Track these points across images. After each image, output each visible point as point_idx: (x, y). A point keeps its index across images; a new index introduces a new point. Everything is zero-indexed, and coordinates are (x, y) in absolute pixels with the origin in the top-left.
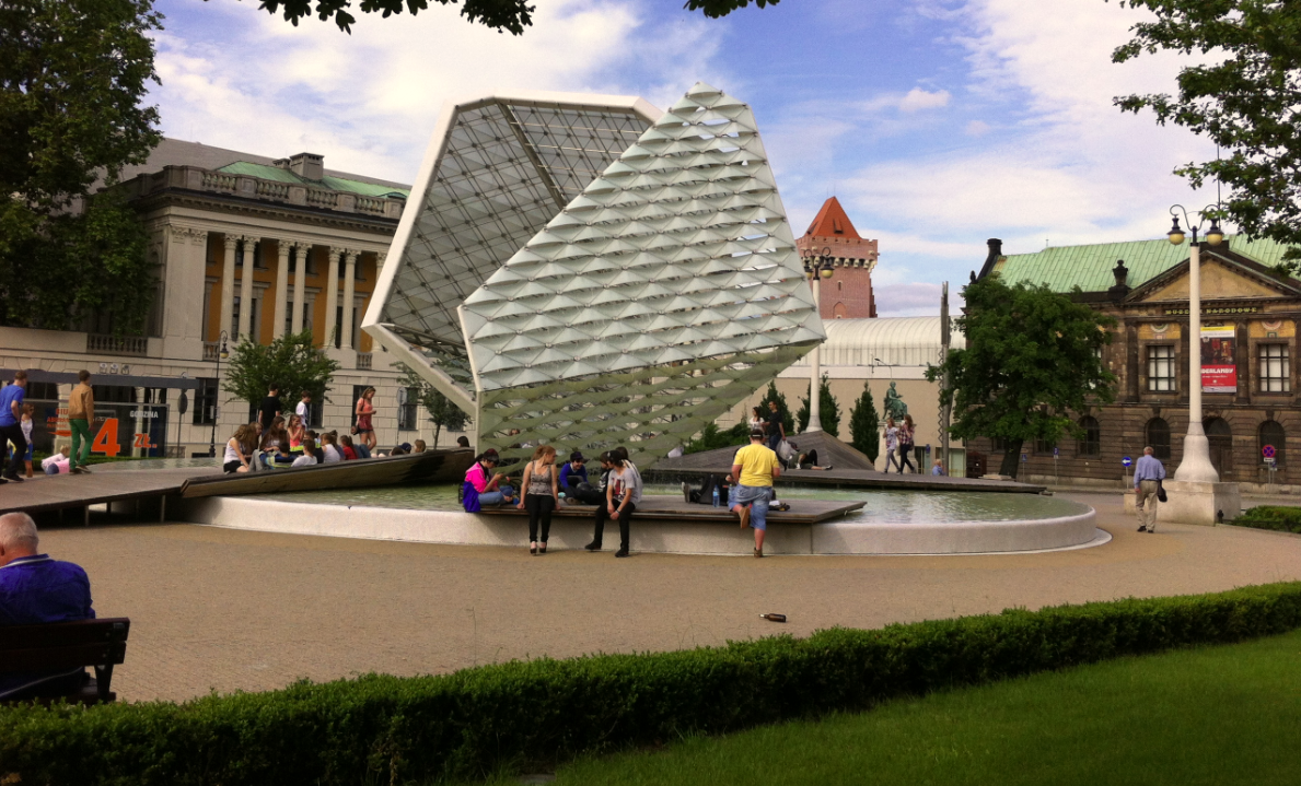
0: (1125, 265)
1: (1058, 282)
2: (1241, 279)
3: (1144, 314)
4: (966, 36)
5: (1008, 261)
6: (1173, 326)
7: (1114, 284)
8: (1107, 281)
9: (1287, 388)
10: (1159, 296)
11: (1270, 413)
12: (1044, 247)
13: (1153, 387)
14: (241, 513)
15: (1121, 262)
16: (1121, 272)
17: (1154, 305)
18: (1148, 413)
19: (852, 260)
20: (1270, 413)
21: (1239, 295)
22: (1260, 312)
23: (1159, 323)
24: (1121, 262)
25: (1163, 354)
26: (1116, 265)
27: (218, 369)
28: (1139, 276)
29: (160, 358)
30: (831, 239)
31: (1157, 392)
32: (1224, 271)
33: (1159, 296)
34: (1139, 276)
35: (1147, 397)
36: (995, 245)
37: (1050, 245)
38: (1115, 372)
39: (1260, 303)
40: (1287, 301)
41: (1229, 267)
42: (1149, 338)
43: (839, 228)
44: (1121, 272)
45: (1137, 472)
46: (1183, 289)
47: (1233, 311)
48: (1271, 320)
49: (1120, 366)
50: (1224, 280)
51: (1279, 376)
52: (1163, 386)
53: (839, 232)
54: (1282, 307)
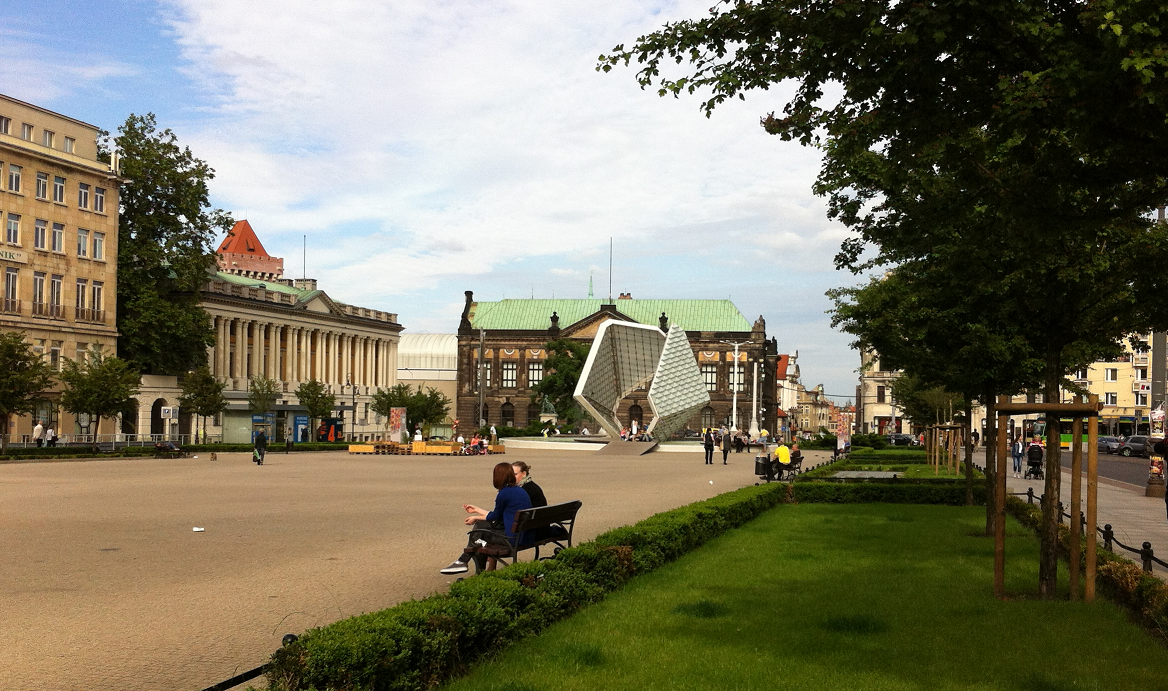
4: (177, 20)
5: (479, 305)
7: (550, 325)
8: (547, 324)
9: (714, 389)
10: (578, 335)
11: (636, 401)
12: (502, 299)
13: (505, 385)
14: (664, 448)
15: (555, 313)
16: (555, 319)
18: (528, 400)
19: (263, 274)
20: (636, 401)
24: (555, 313)
28: (563, 324)
30: (247, 256)
31: (507, 388)
33: (578, 335)
34: (563, 324)
36: (469, 294)
43: (252, 247)
44: (555, 319)
45: (497, 532)
46: (592, 331)
53: (252, 250)
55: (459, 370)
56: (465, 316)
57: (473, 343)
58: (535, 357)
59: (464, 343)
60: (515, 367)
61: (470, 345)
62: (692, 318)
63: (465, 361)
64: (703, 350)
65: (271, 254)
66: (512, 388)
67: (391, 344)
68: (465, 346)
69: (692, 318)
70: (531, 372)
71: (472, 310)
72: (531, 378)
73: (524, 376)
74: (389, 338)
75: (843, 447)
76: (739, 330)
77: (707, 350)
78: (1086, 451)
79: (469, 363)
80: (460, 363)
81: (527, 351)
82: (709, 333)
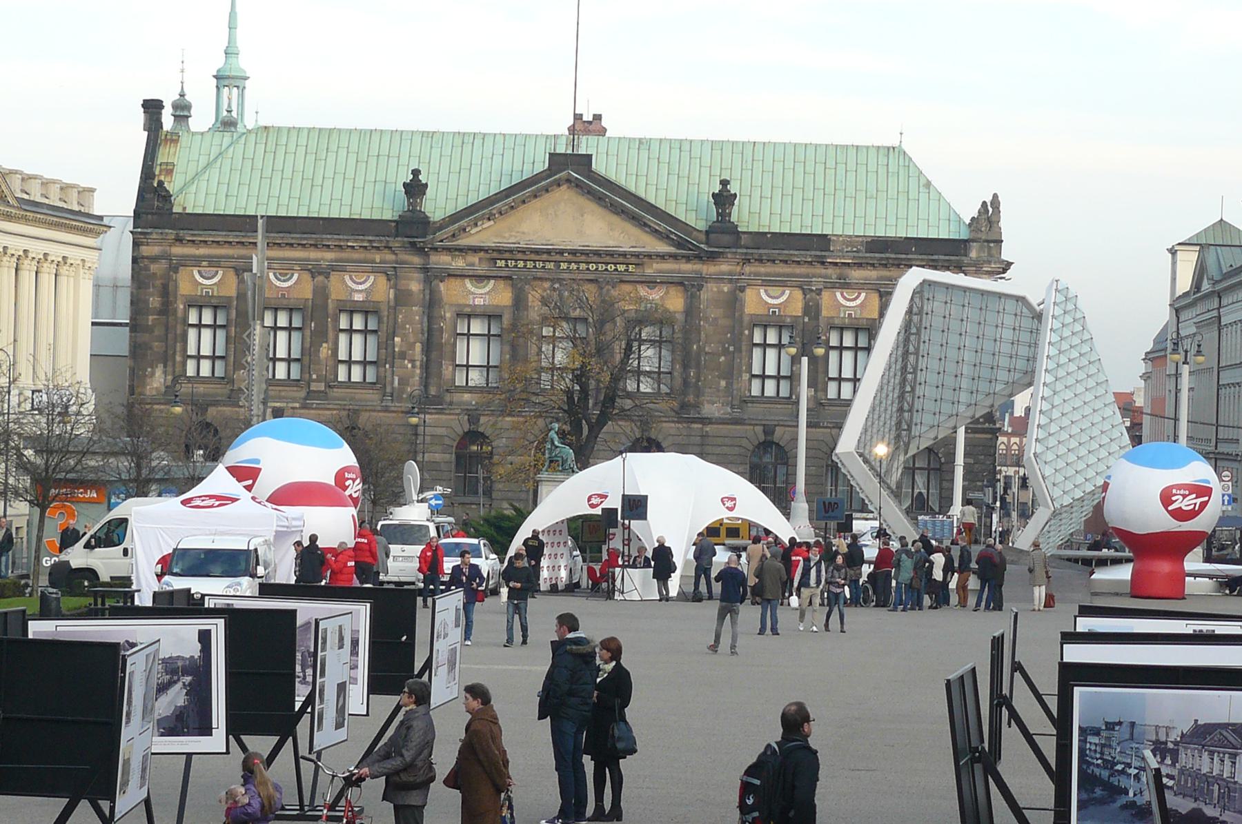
0: (733, 188)
1: (337, 195)
2: (615, 219)
3: (459, 263)
6: (501, 284)
10: (485, 234)
15: (416, 173)
16: (724, 199)
17: (475, 250)
18: (460, 425)
21: (611, 243)
22: (639, 271)
23: (479, 278)
24: (416, 173)
25: (477, 327)
26: (717, 188)
27: (468, 366)
28: (437, 206)
29: (522, 171)
31: (349, 384)
32: (591, 206)
34: (437, 206)
35: (457, 397)
37: (262, 123)
38: (403, 355)
39: (641, 258)
40: (688, 259)
41: (590, 193)
42: (462, 301)
44: (415, 188)
47: (601, 267)
48: (651, 283)
49: (412, 346)
50: (588, 217)
51: (202, 361)
52: (476, 378)
54: (669, 266)
55: (135, 326)
56: (147, 173)
57: (178, 250)
58: (358, 297)
59: (154, 250)
60: (297, 323)
61: (167, 257)
62: (798, 195)
63: (154, 301)
64: (833, 286)
65: (1188, 289)
66: (288, 382)
67: (64, 270)
68: (154, 259)
69: (798, 195)
70: (343, 339)
71: (163, 156)
72: (342, 356)
73: (325, 351)
74: (56, 252)
75: (675, 595)
76: (933, 235)
77: (845, 285)
78: (975, 765)
79: (166, 309)
80: (137, 305)
81: (334, 277)
82: (850, 241)
